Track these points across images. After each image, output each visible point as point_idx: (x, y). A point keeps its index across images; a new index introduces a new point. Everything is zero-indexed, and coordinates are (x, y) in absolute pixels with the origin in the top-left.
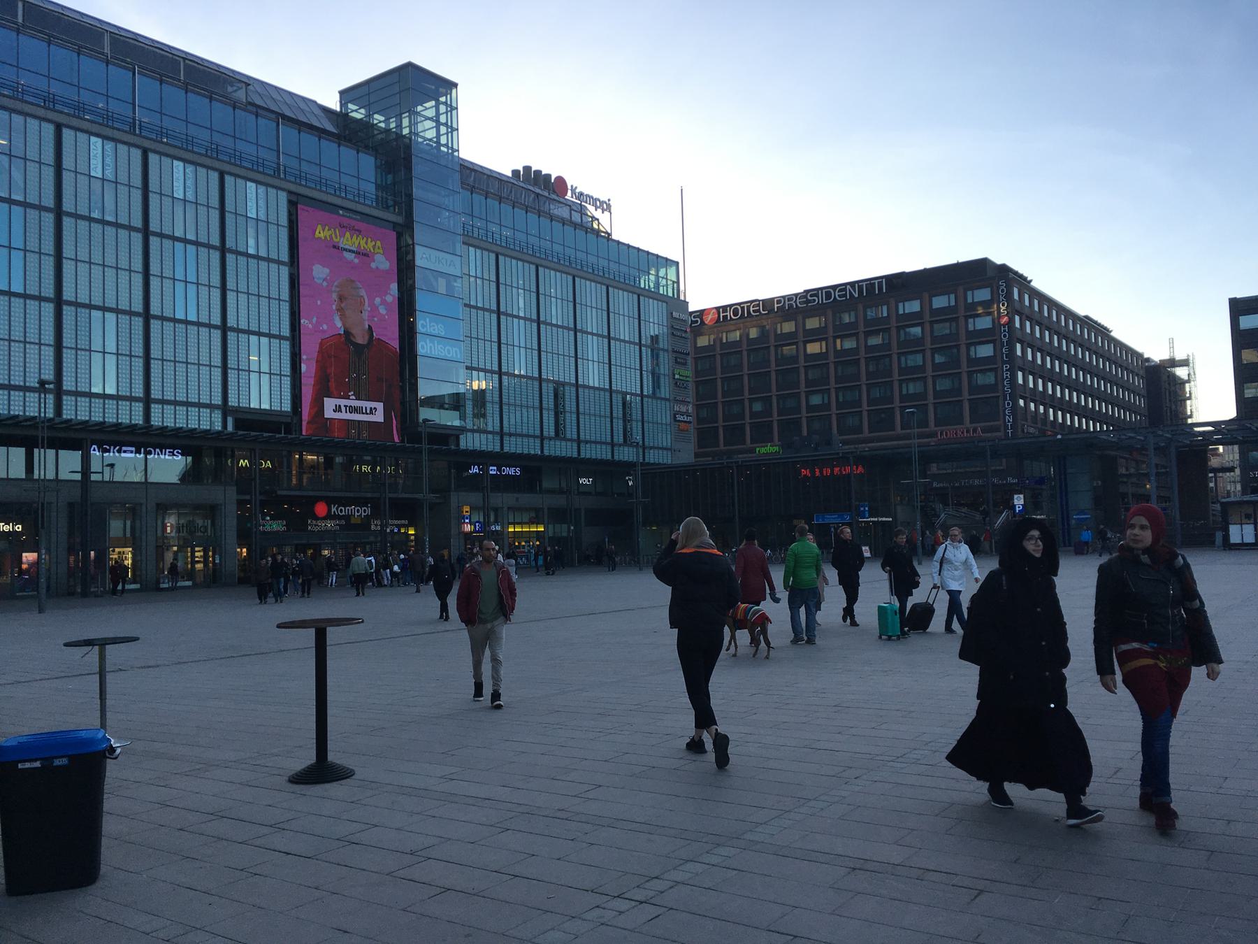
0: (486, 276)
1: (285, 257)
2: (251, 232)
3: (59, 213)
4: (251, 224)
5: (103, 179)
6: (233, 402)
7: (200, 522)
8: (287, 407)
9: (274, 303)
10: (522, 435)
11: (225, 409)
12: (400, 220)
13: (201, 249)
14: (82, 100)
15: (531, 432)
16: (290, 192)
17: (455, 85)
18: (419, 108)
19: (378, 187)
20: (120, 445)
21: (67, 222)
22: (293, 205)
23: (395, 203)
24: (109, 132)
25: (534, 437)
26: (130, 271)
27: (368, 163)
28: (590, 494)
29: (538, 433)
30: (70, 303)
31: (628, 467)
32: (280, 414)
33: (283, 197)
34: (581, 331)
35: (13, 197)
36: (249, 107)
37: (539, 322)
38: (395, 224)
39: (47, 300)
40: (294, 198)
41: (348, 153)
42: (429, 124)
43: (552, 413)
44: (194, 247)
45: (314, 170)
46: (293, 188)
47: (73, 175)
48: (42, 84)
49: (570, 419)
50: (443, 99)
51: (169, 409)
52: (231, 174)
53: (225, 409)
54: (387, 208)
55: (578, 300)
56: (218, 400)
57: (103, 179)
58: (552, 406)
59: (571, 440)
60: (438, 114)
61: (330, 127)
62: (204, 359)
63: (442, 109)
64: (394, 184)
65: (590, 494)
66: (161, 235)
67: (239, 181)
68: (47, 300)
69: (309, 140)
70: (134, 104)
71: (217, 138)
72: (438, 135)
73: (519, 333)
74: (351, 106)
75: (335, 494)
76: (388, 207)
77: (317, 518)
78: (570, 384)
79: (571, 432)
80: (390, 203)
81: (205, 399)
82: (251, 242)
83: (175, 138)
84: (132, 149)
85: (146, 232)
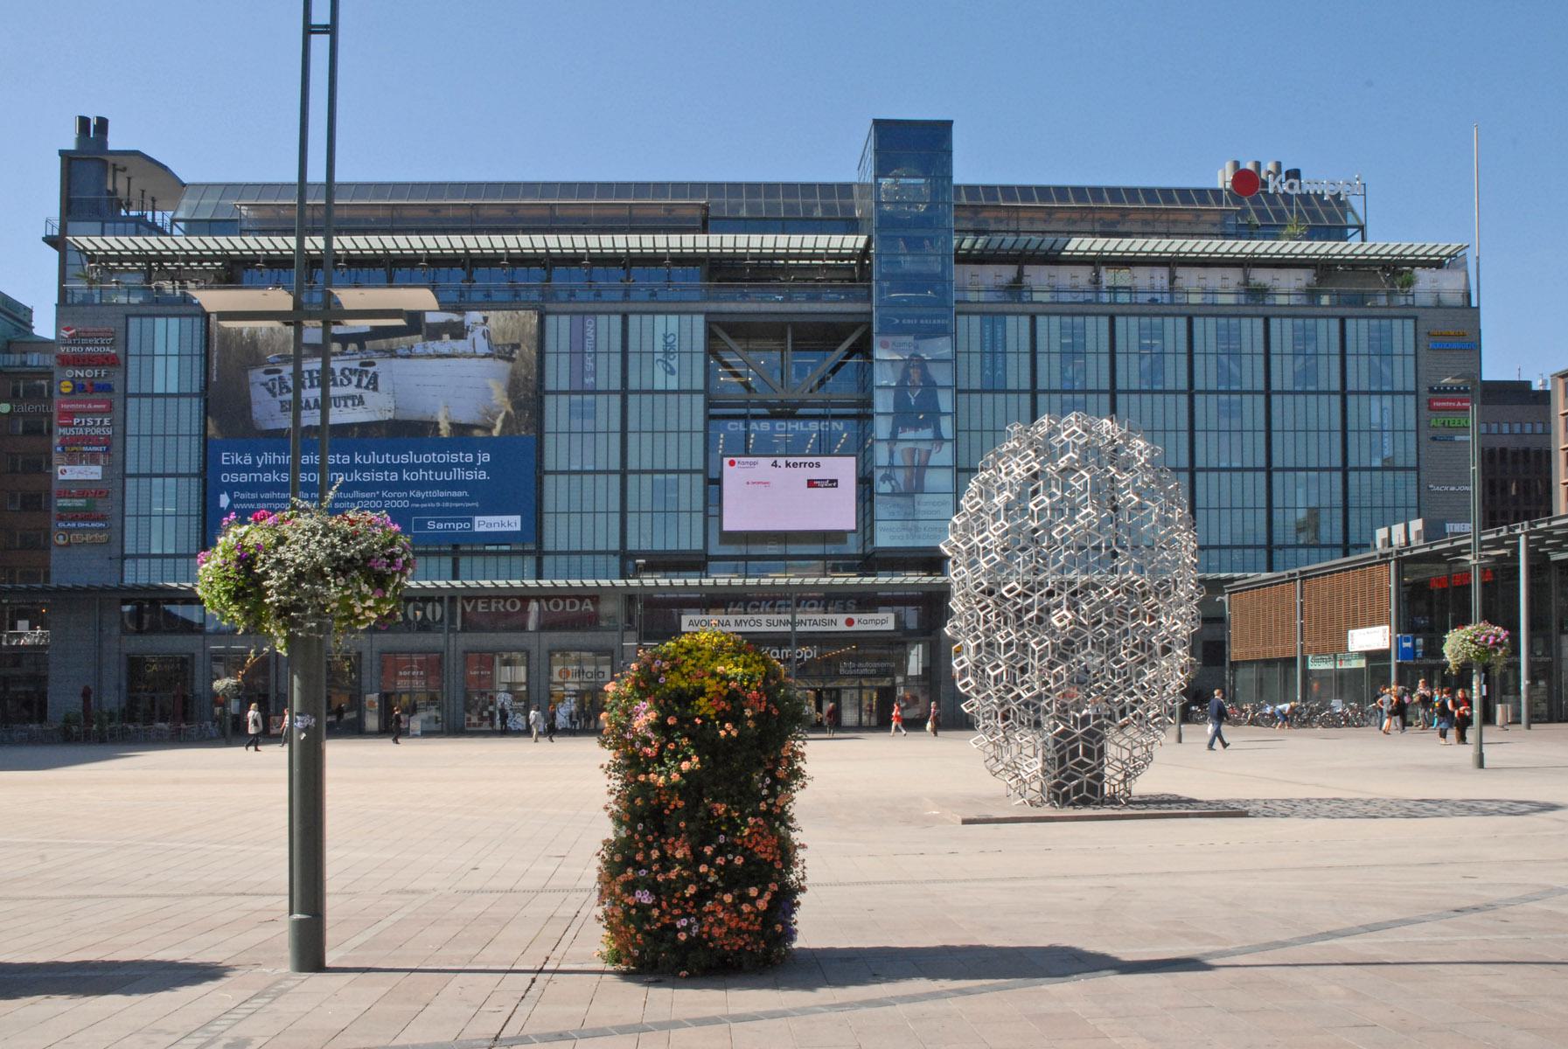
16: (707, 314)
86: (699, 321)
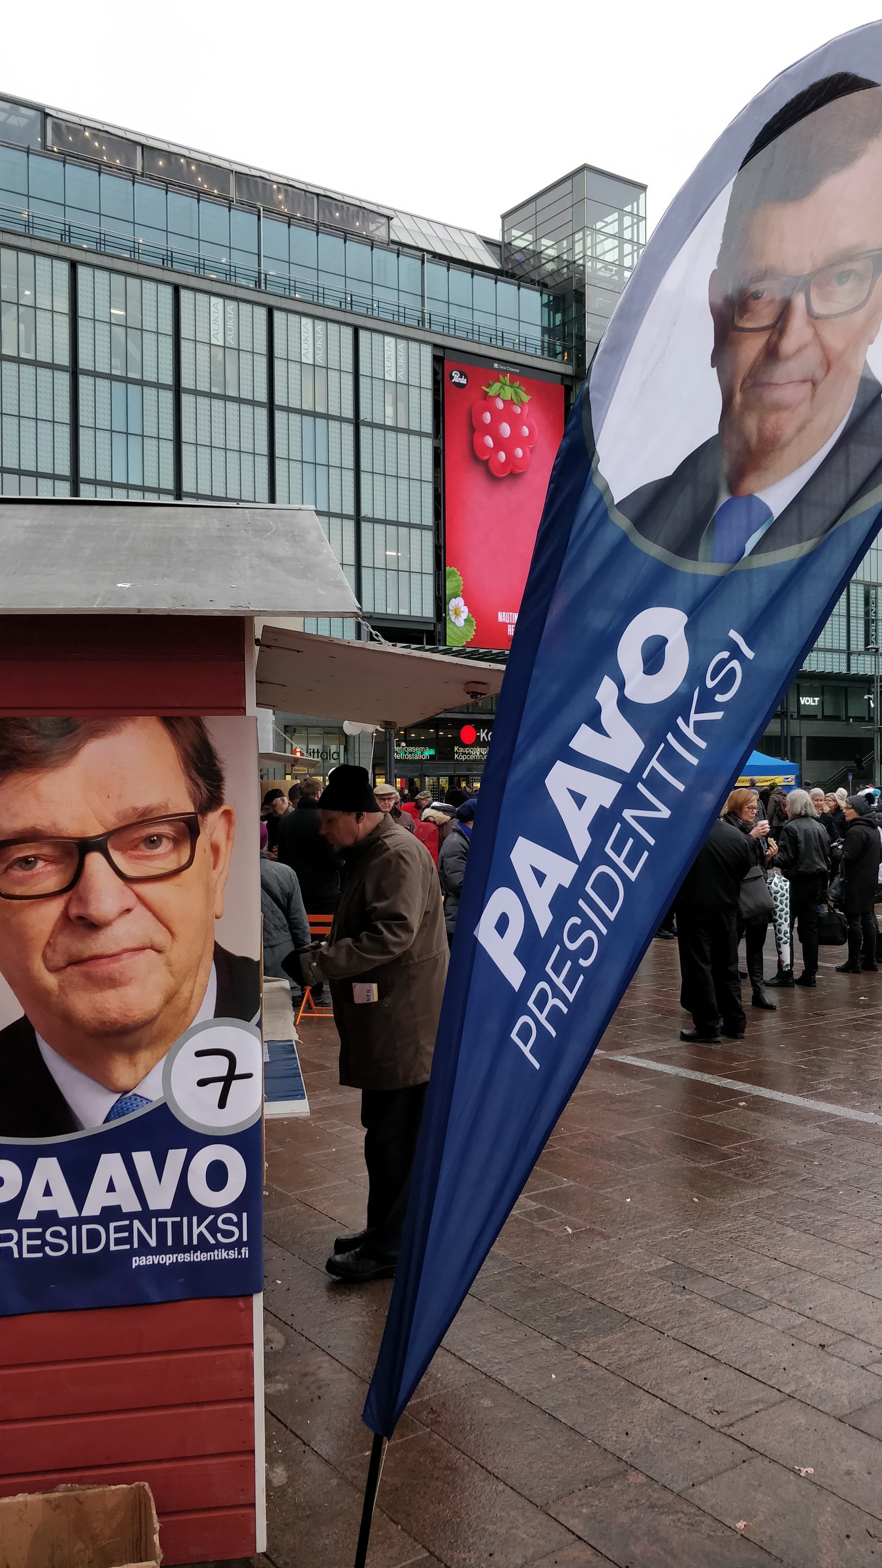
1: (428, 427)
2: (389, 398)
3: (75, 371)
4: (390, 387)
5: (224, 347)
7: (333, 748)
8: (429, 612)
9: (247, 459)
12: (569, 370)
13: (200, 400)
14: (202, 254)
15: (836, 646)
16: (435, 346)
17: (644, 188)
18: (599, 225)
19: (545, 330)
22: (438, 360)
23: (565, 348)
24: (319, 311)
25: (839, 651)
27: (532, 302)
28: (814, 717)
31: (866, 682)
32: (423, 621)
33: (427, 352)
35: (130, 375)
36: (392, 246)
38: (564, 376)
40: (440, 353)
41: (507, 289)
42: (611, 243)
43: (861, 623)
44: (123, 385)
45: (465, 315)
46: (439, 340)
47: (91, 324)
48: (158, 240)
50: (628, 209)
54: (553, 354)
55: (185, 332)
57: (224, 347)
58: (861, 613)
60: (621, 229)
61: (491, 262)
63: (627, 220)
64: (564, 323)
65: (814, 717)
67: (200, 297)
69: (459, 277)
70: (259, 255)
71: (353, 287)
72: (622, 256)
74: (515, 233)
75: (484, 717)
76: (555, 355)
77: (465, 746)
80: (559, 349)
82: (390, 411)
83: (304, 291)
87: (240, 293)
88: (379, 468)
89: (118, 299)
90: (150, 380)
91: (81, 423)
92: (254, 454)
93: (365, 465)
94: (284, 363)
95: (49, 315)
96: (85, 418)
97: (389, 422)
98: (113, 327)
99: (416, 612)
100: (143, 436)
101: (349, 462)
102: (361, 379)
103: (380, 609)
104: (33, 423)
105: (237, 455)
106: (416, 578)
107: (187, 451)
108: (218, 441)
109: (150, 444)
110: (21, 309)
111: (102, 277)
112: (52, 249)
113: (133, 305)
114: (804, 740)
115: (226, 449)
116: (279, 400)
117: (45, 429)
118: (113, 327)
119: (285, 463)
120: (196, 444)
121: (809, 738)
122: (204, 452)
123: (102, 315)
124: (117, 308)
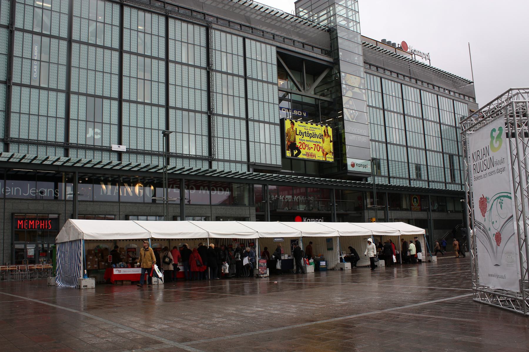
0: (376, 90)
3: (121, 51)
6: (252, 160)
10: (399, 178)
11: (249, 164)
20: (98, 182)
21: (171, 65)
26: (228, 95)
29: (407, 176)
30: (162, 106)
34: (437, 123)
37: (404, 115)
39: (75, 93)
46: (278, 44)
49: (457, 173)
51: (221, 164)
52: (384, 78)
53: (249, 164)
55: (248, 55)
56: (245, 159)
59: (425, 181)
62: (238, 137)
66: (175, 62)
68: (75, 93)
73: (395, 121)
78: (456, 155)
79: (424, 176)
81: (238, 159)
82: (265, 75)
84: (262, 44)
85: (246, 78)
86: (274, 49)
87: (267, 41)
88: (179, 83)
89: (141, 22)
90: (28, 29)
91: (124, 74)
92: (87, 69)
93: (249, 96)
94: (174, 41)
95: (110, 26)
96: (125, 72)
97: (184, 61)
98: (35, 9)
99: (274, 163)
100: (49, 62)
101: (243, 94)
102: (247, 59)
103: (258, 161)
104: (86, 71)
105: (187, 89)
106: (52, 121)
107: (171, 88)
108: (185, 84)
109: (236, 99)
110: (98, 24)
111: (253, 42)
112: (237, 32)
113: (148, 24)
114: (432, 222)
115: (95, 71)
116: (126, 48)
117: (107, 77)
118: (35, 9)
119: (252, 101)
120: (79, 68)
121: (434, 220)
122: (179, 89)
123: (134, 27)
124: (141, 26)
